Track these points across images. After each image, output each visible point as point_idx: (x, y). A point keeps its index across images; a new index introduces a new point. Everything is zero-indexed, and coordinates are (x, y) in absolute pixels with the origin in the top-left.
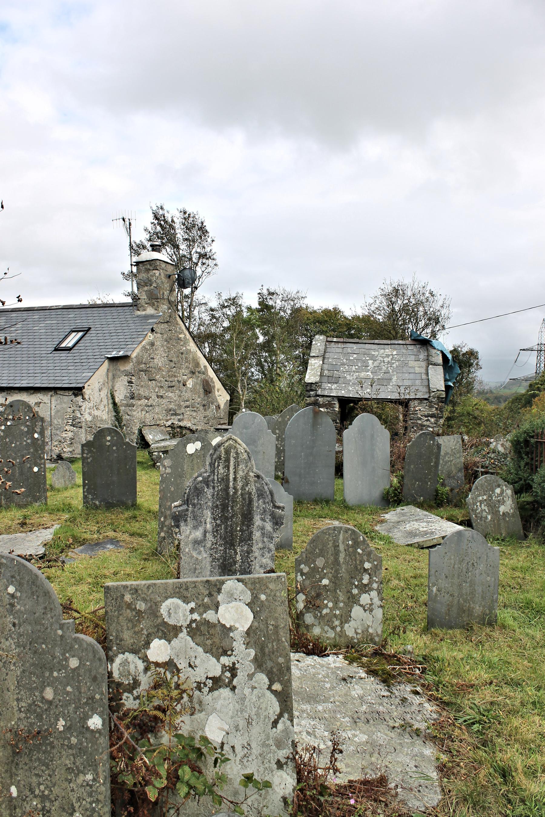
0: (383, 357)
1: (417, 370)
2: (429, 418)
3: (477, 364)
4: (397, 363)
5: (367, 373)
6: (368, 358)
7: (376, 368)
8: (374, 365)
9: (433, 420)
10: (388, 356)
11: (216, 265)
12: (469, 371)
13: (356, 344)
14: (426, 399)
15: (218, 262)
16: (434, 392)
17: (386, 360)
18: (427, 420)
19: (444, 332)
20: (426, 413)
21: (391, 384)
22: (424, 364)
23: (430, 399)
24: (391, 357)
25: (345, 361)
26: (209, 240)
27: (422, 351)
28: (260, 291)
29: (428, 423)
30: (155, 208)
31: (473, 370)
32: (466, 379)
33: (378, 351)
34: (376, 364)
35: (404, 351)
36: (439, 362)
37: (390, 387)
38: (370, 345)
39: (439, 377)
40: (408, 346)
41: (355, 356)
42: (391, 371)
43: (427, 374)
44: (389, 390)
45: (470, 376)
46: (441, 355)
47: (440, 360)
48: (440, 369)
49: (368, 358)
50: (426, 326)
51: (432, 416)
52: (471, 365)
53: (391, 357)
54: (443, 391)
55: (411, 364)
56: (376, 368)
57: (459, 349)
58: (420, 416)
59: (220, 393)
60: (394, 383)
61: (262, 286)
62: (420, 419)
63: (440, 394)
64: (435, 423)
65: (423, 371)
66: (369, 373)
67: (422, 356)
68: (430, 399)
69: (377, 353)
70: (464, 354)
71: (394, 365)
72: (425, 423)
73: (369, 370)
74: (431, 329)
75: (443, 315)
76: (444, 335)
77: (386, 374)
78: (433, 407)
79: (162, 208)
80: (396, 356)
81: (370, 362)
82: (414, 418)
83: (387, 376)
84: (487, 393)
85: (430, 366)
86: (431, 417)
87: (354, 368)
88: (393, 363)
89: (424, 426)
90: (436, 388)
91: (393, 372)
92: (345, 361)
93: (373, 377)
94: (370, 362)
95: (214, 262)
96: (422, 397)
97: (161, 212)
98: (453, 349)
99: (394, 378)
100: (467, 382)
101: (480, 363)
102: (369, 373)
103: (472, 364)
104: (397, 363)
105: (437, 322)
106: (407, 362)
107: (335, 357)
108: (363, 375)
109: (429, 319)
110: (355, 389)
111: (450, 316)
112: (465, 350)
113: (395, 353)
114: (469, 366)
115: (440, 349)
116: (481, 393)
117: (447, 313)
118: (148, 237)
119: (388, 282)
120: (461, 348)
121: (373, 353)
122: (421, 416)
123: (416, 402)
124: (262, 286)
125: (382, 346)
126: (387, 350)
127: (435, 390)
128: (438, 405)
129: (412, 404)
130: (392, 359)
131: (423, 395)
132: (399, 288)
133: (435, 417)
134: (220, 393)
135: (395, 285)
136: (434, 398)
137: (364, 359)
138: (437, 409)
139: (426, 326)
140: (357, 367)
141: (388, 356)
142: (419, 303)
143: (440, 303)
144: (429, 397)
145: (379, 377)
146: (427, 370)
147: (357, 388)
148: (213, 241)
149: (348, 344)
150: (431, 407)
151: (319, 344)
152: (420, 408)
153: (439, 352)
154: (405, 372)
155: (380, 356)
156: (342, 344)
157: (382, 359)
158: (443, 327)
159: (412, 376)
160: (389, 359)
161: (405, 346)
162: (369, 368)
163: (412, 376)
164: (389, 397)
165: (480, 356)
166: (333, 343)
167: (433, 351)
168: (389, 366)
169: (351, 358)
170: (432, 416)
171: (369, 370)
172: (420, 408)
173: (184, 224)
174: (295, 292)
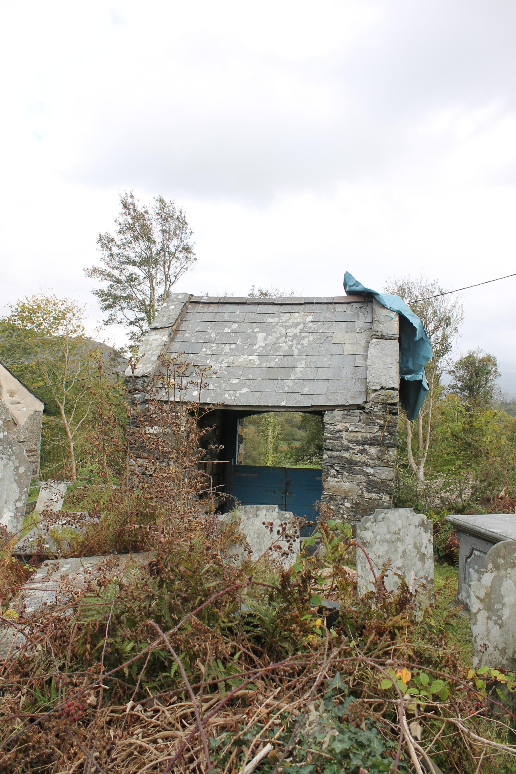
0: (286, 328)
1: (348, 349)
2: (366, 447)
3: (495, 371)
4: (311, 338)
5: (251, 357)
6: (257, 330)
7: (269, 348)
8: (268, 342)
9: (374, 451)
10: (295, 324)
11: (195, 259)
12: (487, 379)
13: (241, 306)
14: (359, 407)
15: (198, 256)
16: (376, 391)
17: (291, 332)
18: (362, 452)
19: (457, 335)
20: (359, 436)
21: (292, 377)
22: (362, 338)
23: (367, 406)
24: (302, 326)
25: (213, 335)
26: (188, 231)
27: (361, 315)
28: (251, 292)
29: (363, 458)
30: (124, 195)
31: (490, 377)
32: (484, 387)
33: (279, 317)
34: (271, 339)
35: (328, 315)
36: (391, 333)
37: (289, 383)
38: (266, 306)
39: (388, 361)
40: (336, 306)
41: (235, 326)
42: (296, 352)
43: (365, 356)
44: (286, 388)
45: (489, 384)
46: (397, 319)
47: (394, 328)
48: (394, 346)
49: (257, 330)
50: (436, 328)
51: (373, 442)
52: (488, 373)
53: (302, 326)
54: (393, 389)
55: (338, 337)
56: (269, 348)
57: (475, 355)
58: (346, 442)
59: (16, 398)
60: (299, 375)
61: (253, 286)
62: (347, 449)
63: (389, 396)
64: (379, 458)
65: (360, 350)
66: (254, 357)
67: (361, 323)
68: (367, 406)
69: (276, 320)
70: (480, 361)
71: (305, 342)
72: (357, 458)
73: (255, 351)
74: (442, 332)
75: (455, 316)
76: (457, 338)
77: (285, 359)
78: (374, 424)
79: (132, 197)
80: (310, 325)
81: (261, 336)
82: (334, 446)
83: (287, 362)
84: (510, 404)
85: (374, 340)
86: (371, 444)
87: (227, 348)
88: (304, 338)
89: (356, 463)
90: (379, 384)
91: (299, 354)
92: (213, 335)
93: (261, 363)
94: (261, 336)
95: (194, 257)
96: (350, 403)
97: (130, 200)
98: (468, 355)
99: (301, 366)
100: (485, 392)
101: (498, 371)
102: (254, 357)
103: (490, 371)
104: (311, 338)
105: (448, 324)
106: (330, 334)
107: (198, 329)
108: (241, 360)
109: (441, 320)
110: (220, 387)
111: (464, 316)
112: (481, 356)
113: (310, 318)
114: (487, 374)
115: (396, 308)
116: (504, 404)
117: (460, 314)
118: (118, 228)
119: (393, 281)
120: (477, 354)
121: (269, 320)
122: (349, 441)
123: (338, 413)
124: (253, 286)
125: (290, 307)
126: (296, 315)
127: (378, 388)
128: (385, 419)
129: (328, 417)
130: (302, 331)
131: (353, 398)
132: (406, 287)
133: (379, 445)
134: (16, 398)
135: (400, 283)
136: (376, 403)
137: (250, 331)
138: (381, 427)
139: (436, 328)
140: (233, 346)
141: (295, 324)
142: (428, 303)
143: (451, 303)
144: (366, 402)
145: (272, 364)
146: (367, 348)
147: (224, 385)
148: (192, 232)
149: (227, 306)
150: (370, 423)
151: (172, 307)
152: (347, 425)
153: (393, 315)
154: (324, 353)
155: (281, 326)
156: (216, 306)
157: (284, 331)
158: (456, 330)
159: (336, 361)
160: (297, 331)
161: (331, 306)
162: (256, 347)
163: (336, 361)
164: (283, 404)
165: (498, 362)
166: (201, 305)
167: (381, 313)
168: (295, 342)
169: (227, 330)
170: (373, 442)
171: (255, 351)
172: (347, 425)
173: (159, 214)
174: (289, 293)
